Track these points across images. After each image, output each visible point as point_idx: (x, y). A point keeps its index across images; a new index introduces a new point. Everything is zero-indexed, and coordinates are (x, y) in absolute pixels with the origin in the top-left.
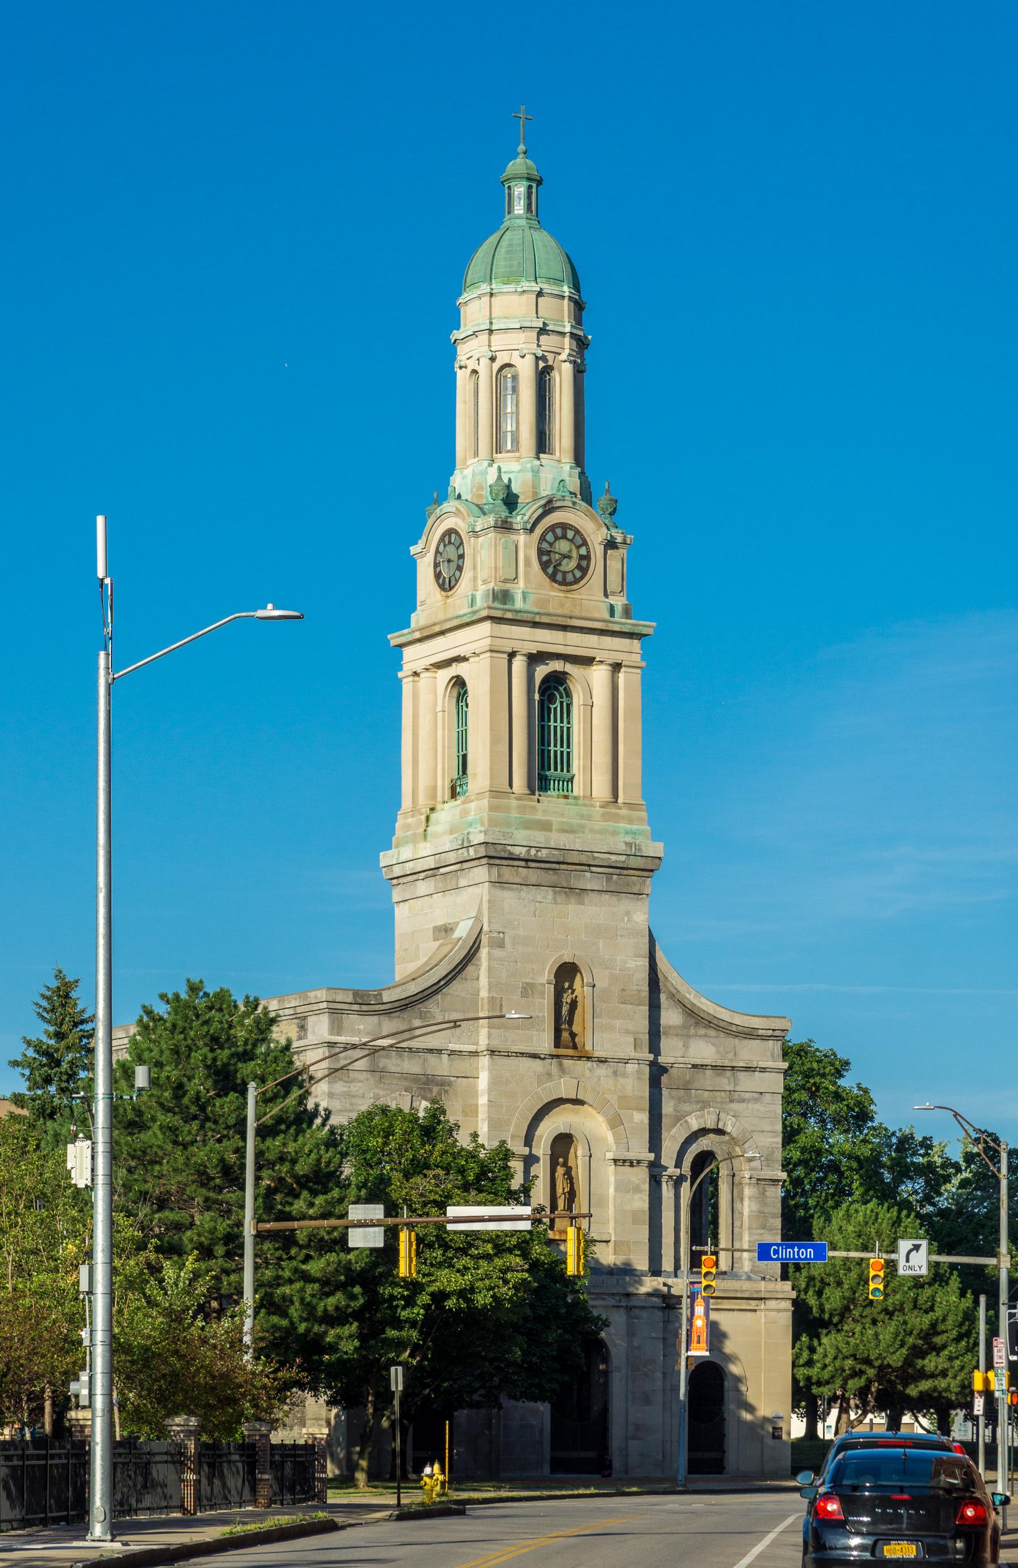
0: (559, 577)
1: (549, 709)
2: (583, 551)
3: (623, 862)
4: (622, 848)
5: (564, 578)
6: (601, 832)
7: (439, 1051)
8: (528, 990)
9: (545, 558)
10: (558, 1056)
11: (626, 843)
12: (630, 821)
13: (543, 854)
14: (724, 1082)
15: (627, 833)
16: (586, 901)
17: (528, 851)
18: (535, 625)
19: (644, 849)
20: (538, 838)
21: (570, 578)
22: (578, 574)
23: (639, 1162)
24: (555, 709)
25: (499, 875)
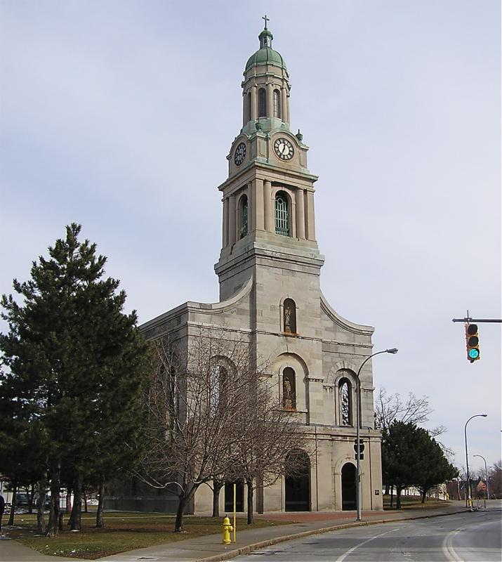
7: (236, 331)
8: (273, 308)
10: (285, 336)
13: (278, 255)
14: (350, 350)
18: (274, 171)
21: (286, 158)
23: (319, 380)
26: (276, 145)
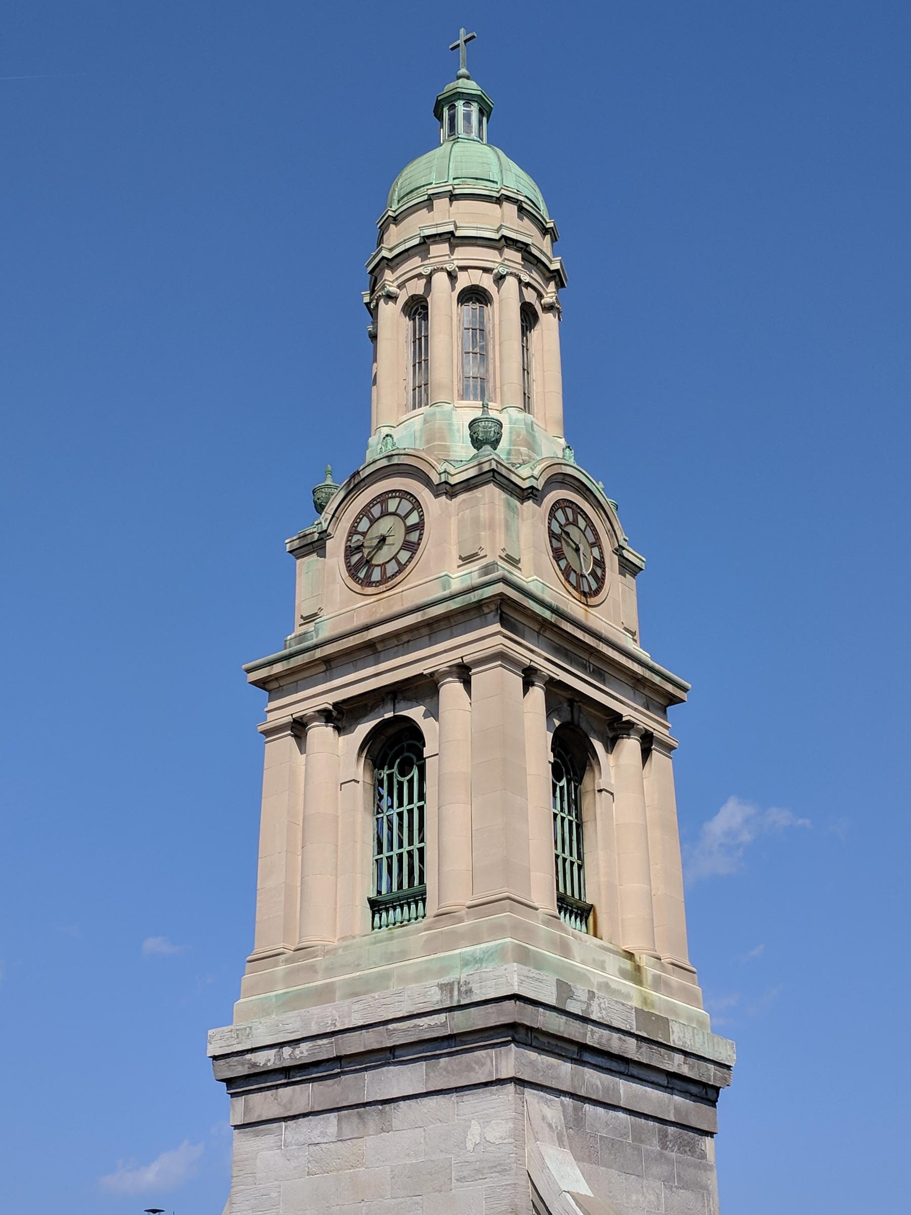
0: (376, 575)
1: (401, 784)
2: (413, 519)
3: (444, 1025)
4: (435, 999)
5: (384, 573)
6: (419, 977)
9: (355, 558)
11: (442, 987)
12: (475, 937)
13: (304, 1053)
15: (466, 964)
16: (396, 1123)
17: (280, 1056)
19: (475, 987)
20: (293, 1024)
22: (404, 556)
24: (411, 782)
25: (247, 1110)
26: (392, 505)
